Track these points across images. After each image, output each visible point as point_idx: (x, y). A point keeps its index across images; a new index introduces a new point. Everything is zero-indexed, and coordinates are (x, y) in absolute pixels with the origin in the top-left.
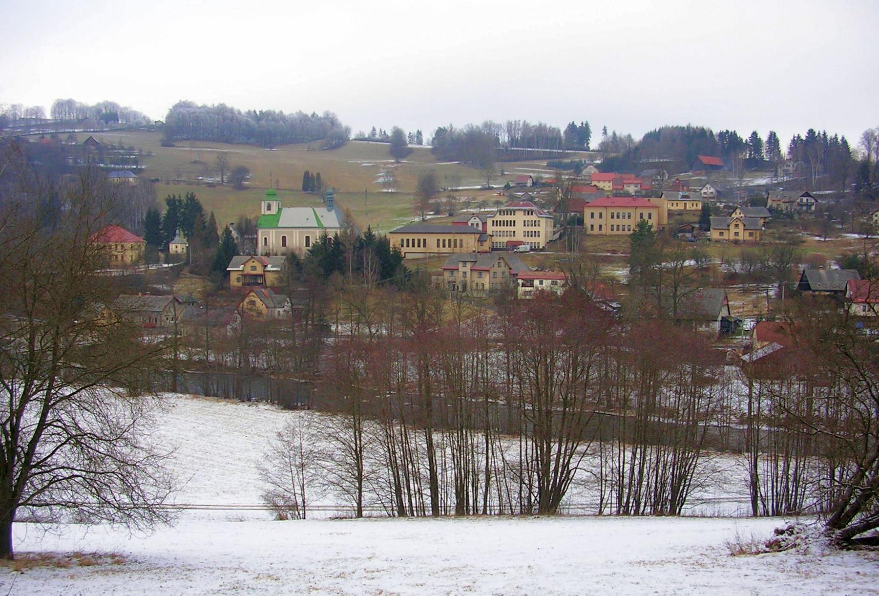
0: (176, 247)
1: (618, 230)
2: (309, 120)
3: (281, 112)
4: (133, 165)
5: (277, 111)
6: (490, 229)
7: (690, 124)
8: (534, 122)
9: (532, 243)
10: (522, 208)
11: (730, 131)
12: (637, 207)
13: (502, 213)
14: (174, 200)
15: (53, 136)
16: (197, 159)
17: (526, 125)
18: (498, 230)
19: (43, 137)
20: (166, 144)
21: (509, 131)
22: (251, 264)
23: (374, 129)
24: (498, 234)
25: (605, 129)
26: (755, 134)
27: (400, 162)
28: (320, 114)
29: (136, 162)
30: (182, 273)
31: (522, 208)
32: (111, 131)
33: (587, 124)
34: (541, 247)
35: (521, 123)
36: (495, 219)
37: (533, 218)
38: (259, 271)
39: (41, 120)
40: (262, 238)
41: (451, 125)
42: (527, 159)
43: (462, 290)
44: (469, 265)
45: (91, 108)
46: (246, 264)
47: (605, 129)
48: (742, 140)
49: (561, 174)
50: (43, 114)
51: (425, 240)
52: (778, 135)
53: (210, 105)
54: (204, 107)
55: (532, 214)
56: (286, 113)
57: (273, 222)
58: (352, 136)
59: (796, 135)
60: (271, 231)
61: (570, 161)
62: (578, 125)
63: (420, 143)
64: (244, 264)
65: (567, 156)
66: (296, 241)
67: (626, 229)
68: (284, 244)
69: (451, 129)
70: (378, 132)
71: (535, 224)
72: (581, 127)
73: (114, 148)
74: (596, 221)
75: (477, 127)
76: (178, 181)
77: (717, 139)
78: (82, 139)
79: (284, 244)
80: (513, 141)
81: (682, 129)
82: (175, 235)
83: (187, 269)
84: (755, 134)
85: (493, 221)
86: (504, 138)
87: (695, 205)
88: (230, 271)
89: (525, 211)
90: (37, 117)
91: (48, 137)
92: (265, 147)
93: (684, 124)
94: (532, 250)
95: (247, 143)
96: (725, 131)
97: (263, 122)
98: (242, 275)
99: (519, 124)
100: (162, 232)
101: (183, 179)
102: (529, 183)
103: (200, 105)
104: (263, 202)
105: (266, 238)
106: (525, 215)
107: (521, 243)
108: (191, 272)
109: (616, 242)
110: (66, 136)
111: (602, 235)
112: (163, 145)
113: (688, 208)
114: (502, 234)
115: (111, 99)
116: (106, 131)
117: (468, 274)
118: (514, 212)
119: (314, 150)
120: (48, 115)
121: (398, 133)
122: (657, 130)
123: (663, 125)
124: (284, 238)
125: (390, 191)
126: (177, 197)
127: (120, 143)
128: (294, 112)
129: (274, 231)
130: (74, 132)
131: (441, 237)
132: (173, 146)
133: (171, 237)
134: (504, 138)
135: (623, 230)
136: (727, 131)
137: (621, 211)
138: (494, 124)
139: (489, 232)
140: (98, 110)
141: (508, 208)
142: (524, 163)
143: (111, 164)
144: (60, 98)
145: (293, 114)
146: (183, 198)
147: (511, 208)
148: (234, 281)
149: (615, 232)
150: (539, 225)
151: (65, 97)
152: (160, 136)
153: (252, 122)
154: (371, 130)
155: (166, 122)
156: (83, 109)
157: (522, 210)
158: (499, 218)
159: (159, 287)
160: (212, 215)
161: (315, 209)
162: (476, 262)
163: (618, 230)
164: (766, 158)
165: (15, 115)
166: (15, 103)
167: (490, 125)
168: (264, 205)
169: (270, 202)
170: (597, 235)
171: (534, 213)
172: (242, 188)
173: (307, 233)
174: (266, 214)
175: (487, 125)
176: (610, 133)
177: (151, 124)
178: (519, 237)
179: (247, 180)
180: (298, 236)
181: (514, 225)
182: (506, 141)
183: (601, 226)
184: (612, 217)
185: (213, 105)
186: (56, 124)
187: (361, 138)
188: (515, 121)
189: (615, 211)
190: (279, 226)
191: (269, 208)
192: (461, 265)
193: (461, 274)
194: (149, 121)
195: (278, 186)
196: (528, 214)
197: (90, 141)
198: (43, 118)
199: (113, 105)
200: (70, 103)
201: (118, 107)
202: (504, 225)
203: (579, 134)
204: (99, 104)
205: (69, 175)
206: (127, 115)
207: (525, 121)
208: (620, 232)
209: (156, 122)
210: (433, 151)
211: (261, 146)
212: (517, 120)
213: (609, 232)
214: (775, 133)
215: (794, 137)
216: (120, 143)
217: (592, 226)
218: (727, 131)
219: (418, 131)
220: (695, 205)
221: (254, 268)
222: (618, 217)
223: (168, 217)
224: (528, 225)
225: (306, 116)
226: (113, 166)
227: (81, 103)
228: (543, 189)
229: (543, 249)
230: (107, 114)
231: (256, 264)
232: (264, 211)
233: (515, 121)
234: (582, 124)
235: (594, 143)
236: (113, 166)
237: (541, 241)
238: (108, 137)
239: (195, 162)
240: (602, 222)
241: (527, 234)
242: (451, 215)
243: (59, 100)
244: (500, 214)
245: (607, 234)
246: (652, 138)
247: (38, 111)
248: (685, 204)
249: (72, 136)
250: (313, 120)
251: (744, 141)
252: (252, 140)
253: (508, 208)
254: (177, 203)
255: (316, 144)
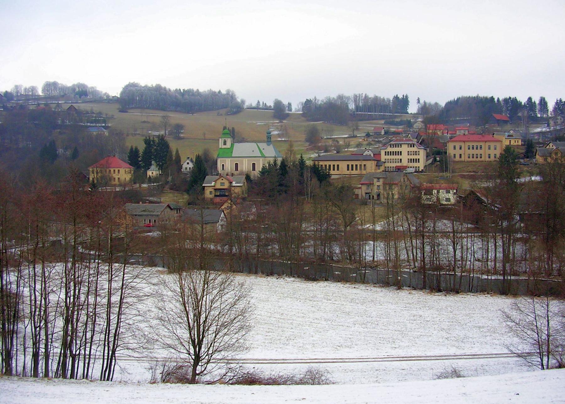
0: (152, 173)
1: (473, 157)
2: (217, 95)
3: (198, 90)
4: (103, 124)
5: (195, 90)
6: (383, 157)
7: (478, 95)
8: (371, 95)
9: (416, 167)
10: (406, 142)
11: (512, 98)
12: (486, 142)
13: (392, 146)
14: (150, 141)
15: (46, 105)
16: (146, 120)
17: (366, 97)
18: (392, 158)
19: (39, 106)
20: (122, 111)
21: (355, 101)
22: (220, 181)
23: (259, 102)
24: (412, 153)
25: (419, 100)
26: (530, 99)
27: (282, 122)
28: (224, 92)
29: (104, 122)
30: (165, 189)
31: (406, 142)
32: (83, 102)
33: (407, 96)
34: (420, 170)
35: (364, 96)
36: (387, 151)
37: (415, 149)
38: (226, 186)
39: (35, 96)
40: (220, 166)
41: (315, 97)
42: (368, 120)
43: (376, 199)
44: (381, 180)
45: (68, 88)
46: (217, 181)
47: (419, 100)
48: (521, 103)
49: (390, 128)
50: (37, 91)
51: (338, 166)
52: (546, 99)
53: (149, 85)
54: (146, 86)
55: (414, 147)
56: (201, 90)
57: (228, 153)
58: (245, 107)
59: (559, 99)
60: (227, 159)
61: (400, 120)
62: (400, 96)
63: (291, 110)
64: (215, 181)
65: (396, 117)
66: (245, 166)
67: (479, 157)
68: (237, 169)
69: (315, 100)
70: (261, 103)
71: (416, 153)
72: (403, 98)
73: (87, 113)
74: (458, 152)
75: (333, 98)
76: (135, 134)
77: (502, 103)
78: (66, 107)
79: (237, 169)
80: (357, 108)
81: (474, 98)
82: (151, 165)
83: (167, 186)
84: (530, 99)
85: (386, 152)
86: (352, 106)
87: (517, 142)
88: (205, 186)
89: (408, 144)
90: (32, 93)
91: (42, 106)
92: (188, 113)
93: (474, 95)
94: (415, 172)
95: (176, 111)
96: (508, 98)
97: (187, 96)
98: (215, 189)
99: (362, 96)
100: (140, 163)
101: (138, 132)
102: (383, 133)
103: (143, 85)
104: (220, 140)
105: (223, 165)
106: (408, 147)
107: (406, 167)
108: (171, 189)
109: (474, 165)
110: (54, 106)
111: (461, 162)
112: (120, 111)
113: (512, 144)
114: (391, 161)
115: (82, 82)
116: (79, 103)
117: (381, 187)
118: (401, 145)
119: (221, 115)
120: (40, 93)
121: (278, 104)
122: (456, 99)
123: (460, 96)
124: (237, 164)
125: (283, 139)
126: (151, 139)
127: (92, 110)
128: (206, 90)
129: (229, 159)
130: (58, 103)
131: (350, 163)
132: (127, 112)
133: (148, 166)
134: (352, 106)
135: (477, 158)
136: (510, 98)
137: (475, 144)
138: (345, 96)
139: (383, 160)
140: (73, 89)
141: (396, 142)
142: (367, 122)
143: (88, 123)
144: (48, 81)
145: (205, 92)
146: (156, 140)
147: (398, 142)
148: (208, 194)
149: (471, 159)
150: (419, 154)
151: (52, 80)
152: (117, 106)
153: (179, 97)
154: (256, 102)
155: (120, 96)
156: (64, 89)
157: (406, 144)
158: (389, 149)
159: (151, 199)
160: (177, 151)
161: (258, 144)
162: (386, 178)
163: (473, 157)
164: (539, 115)
165: (17, 92)
166: (17, 84)
167: (342, 97)
168: (221, 141)
169: (226, 139)
170: (458, 161)
171: (415, 146)
172: (179, 138)
173: (254, 161)
174: (222, 147)
175: (340, 97)
176: (422, 102)
177: (110, 98)
178: (405, 163)
179: (182, 133)
180: (246, 162)
181: (401, 155)
182: (353, 108)
183: (460, 155)
184: (469, 149)
185: (152, 85)
186: (45, 98)
187: (251, 108)
188: (359, 94)
189: (471, 144)
190: (233, 156)
191: (225, 143)
192: (375, 180)
193: (376, 187)
194: (108, 96)
195: (205, 137)
196: (411, 147)
197: (71, 108)
198: (37, 94)
199: (84, 86)
200: (55, 84)
201: (87, 87)
202: (396, 155)
203: (403, 103)
204: (74, 85)
205: (59, 130)
206: (94, 92)
207: (366, 94)
208: (475, 159)
209: (113, 97)
210: (303, 115)
211: (185, 113)
212: (361, 93)
213: (467, 159)
214: (544, 98)
215: (557, 101)
216: (92, 110)
217: (455, 155)
218: (510, 98)
219: (289, 103)
220: (517, 142)
221: (222, 184)
222: (473, 148)
223: (145, 152)
224: (411, 155)
225: (215, 92)
226: (89, 124)
227: (62, 84)
228: (394, 136)
229: (422, 171)
230: (79, 91)
231: (224, 181)
232: (221, 145)
233: (359, 94)
234: (403, 96)
235: (413, 109)
236: (89, 124)
237: (421, 165)
238: (82, 106)
239: (144, 122)
240: (461, 152)
241: (411, 161)
242: (338, 152)
243: (47, 82)
244: (391, 147)
245: (466, 161)
246: (450, 105)
247: (33, 89)
248: (510, 141)
249: (58, 105)
250: (219, 95)
251: (523, 104)
252: (179, 109)
253: (396, 142)
254: (152, 143)
255: (223, 111)
